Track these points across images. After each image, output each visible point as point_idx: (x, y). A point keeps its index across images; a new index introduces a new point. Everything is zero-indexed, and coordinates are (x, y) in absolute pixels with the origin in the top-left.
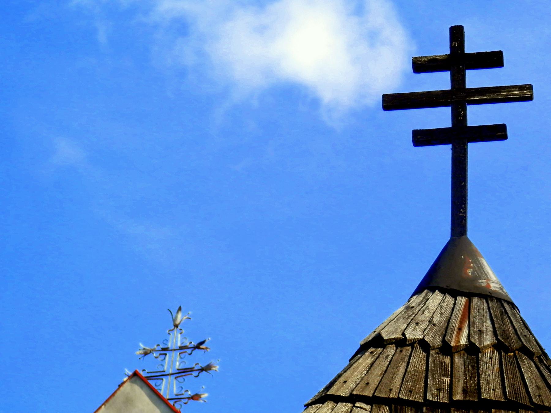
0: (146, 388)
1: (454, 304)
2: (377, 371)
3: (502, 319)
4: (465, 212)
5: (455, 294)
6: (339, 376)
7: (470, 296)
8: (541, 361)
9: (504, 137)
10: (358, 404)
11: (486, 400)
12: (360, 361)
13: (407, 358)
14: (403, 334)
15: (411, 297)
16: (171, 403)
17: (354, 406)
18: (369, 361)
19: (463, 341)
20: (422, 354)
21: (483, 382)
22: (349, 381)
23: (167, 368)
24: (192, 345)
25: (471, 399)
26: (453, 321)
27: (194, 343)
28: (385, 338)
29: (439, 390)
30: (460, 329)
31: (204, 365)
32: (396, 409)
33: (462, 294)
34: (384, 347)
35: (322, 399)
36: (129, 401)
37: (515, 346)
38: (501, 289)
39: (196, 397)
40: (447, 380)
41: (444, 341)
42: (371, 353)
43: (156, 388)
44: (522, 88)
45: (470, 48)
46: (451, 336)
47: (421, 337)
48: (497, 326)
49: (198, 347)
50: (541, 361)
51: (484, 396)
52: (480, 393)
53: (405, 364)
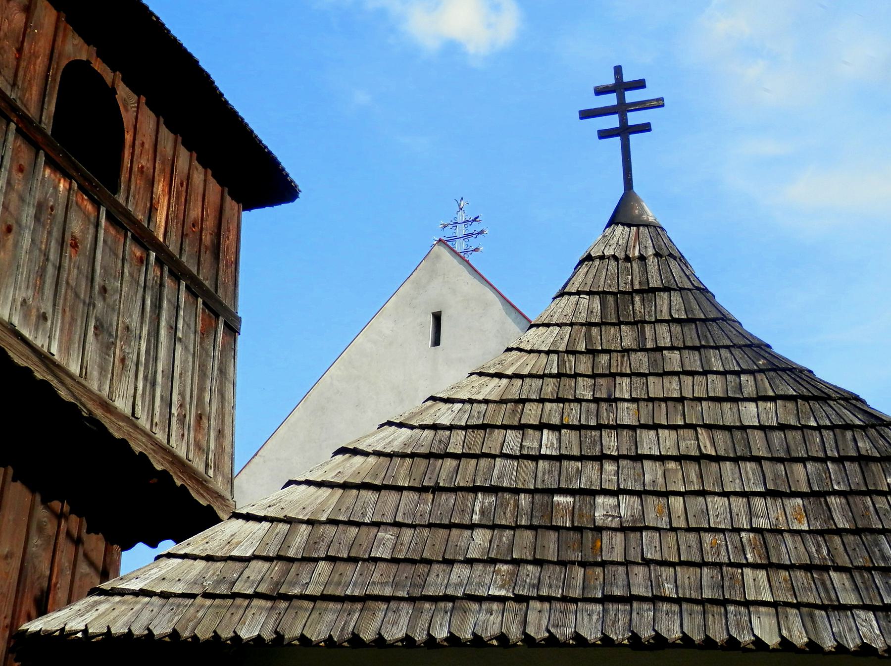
0: (447, 248)
1: (630, 232)
2: (591, 276)
3: (657, 238)
4: (631, 176)
5: (630, 226)
6: (570, 279)
7: (638, 226)
8: (681, 260)
9: (650, 130)
10: (581, 296)
11: (652, 287)
12: (580, 270)
13: (606, 267)
14: (603, 253)
15: (605, 229)
16: (462, 254)
17: (580, 297)
18: (586, 270)
19: (637, 254)
20: (615, 263)
21: (650, 277)
22: (576, 283)
23: (458, 235)
24: (471, 220)
25: (644, 288)
26: (629, 242)
27: (473, 218)
28: (593, 256)
29: (626, 284)
30: (634, 247)
31: (479, 230)
32: (603, 296)
33: (634, 225)
34: (593, 261)
35: (562, 294)
36: (438, 257)
37: (666, 253)
38: (656, 220)
39: (476, 250)
40: (630, 277)
41: (626, 255)
42: (586, 265)
43: (452, 246)
44: (658, 100)
45: (626, 78)
46: (630, 251)
47: (613, 253)
48: (654, 243)
49: (475, 220)
50: (681, 260)
51: (651, 285)
52: (648, 284)
53: (605, 270)
